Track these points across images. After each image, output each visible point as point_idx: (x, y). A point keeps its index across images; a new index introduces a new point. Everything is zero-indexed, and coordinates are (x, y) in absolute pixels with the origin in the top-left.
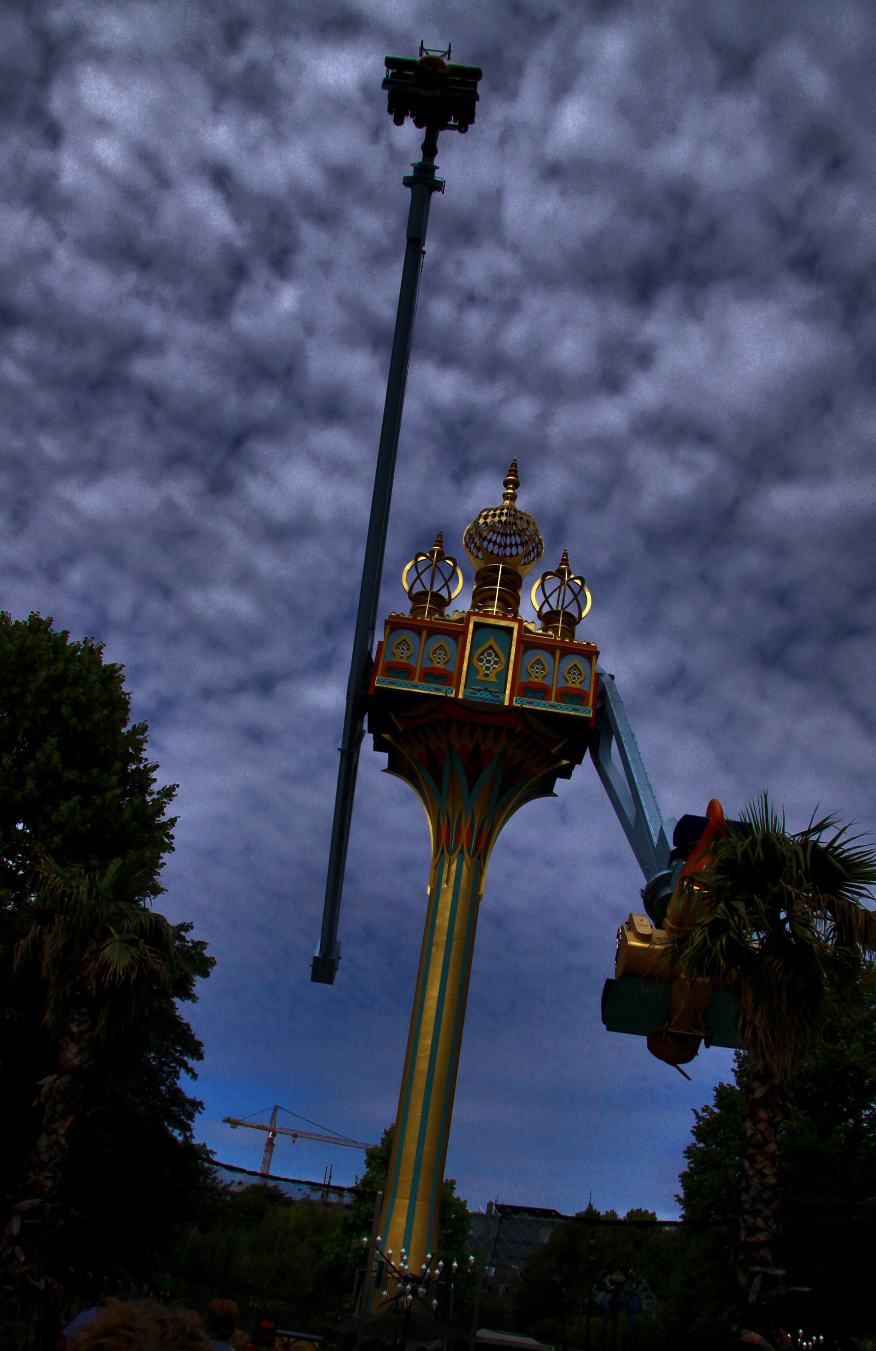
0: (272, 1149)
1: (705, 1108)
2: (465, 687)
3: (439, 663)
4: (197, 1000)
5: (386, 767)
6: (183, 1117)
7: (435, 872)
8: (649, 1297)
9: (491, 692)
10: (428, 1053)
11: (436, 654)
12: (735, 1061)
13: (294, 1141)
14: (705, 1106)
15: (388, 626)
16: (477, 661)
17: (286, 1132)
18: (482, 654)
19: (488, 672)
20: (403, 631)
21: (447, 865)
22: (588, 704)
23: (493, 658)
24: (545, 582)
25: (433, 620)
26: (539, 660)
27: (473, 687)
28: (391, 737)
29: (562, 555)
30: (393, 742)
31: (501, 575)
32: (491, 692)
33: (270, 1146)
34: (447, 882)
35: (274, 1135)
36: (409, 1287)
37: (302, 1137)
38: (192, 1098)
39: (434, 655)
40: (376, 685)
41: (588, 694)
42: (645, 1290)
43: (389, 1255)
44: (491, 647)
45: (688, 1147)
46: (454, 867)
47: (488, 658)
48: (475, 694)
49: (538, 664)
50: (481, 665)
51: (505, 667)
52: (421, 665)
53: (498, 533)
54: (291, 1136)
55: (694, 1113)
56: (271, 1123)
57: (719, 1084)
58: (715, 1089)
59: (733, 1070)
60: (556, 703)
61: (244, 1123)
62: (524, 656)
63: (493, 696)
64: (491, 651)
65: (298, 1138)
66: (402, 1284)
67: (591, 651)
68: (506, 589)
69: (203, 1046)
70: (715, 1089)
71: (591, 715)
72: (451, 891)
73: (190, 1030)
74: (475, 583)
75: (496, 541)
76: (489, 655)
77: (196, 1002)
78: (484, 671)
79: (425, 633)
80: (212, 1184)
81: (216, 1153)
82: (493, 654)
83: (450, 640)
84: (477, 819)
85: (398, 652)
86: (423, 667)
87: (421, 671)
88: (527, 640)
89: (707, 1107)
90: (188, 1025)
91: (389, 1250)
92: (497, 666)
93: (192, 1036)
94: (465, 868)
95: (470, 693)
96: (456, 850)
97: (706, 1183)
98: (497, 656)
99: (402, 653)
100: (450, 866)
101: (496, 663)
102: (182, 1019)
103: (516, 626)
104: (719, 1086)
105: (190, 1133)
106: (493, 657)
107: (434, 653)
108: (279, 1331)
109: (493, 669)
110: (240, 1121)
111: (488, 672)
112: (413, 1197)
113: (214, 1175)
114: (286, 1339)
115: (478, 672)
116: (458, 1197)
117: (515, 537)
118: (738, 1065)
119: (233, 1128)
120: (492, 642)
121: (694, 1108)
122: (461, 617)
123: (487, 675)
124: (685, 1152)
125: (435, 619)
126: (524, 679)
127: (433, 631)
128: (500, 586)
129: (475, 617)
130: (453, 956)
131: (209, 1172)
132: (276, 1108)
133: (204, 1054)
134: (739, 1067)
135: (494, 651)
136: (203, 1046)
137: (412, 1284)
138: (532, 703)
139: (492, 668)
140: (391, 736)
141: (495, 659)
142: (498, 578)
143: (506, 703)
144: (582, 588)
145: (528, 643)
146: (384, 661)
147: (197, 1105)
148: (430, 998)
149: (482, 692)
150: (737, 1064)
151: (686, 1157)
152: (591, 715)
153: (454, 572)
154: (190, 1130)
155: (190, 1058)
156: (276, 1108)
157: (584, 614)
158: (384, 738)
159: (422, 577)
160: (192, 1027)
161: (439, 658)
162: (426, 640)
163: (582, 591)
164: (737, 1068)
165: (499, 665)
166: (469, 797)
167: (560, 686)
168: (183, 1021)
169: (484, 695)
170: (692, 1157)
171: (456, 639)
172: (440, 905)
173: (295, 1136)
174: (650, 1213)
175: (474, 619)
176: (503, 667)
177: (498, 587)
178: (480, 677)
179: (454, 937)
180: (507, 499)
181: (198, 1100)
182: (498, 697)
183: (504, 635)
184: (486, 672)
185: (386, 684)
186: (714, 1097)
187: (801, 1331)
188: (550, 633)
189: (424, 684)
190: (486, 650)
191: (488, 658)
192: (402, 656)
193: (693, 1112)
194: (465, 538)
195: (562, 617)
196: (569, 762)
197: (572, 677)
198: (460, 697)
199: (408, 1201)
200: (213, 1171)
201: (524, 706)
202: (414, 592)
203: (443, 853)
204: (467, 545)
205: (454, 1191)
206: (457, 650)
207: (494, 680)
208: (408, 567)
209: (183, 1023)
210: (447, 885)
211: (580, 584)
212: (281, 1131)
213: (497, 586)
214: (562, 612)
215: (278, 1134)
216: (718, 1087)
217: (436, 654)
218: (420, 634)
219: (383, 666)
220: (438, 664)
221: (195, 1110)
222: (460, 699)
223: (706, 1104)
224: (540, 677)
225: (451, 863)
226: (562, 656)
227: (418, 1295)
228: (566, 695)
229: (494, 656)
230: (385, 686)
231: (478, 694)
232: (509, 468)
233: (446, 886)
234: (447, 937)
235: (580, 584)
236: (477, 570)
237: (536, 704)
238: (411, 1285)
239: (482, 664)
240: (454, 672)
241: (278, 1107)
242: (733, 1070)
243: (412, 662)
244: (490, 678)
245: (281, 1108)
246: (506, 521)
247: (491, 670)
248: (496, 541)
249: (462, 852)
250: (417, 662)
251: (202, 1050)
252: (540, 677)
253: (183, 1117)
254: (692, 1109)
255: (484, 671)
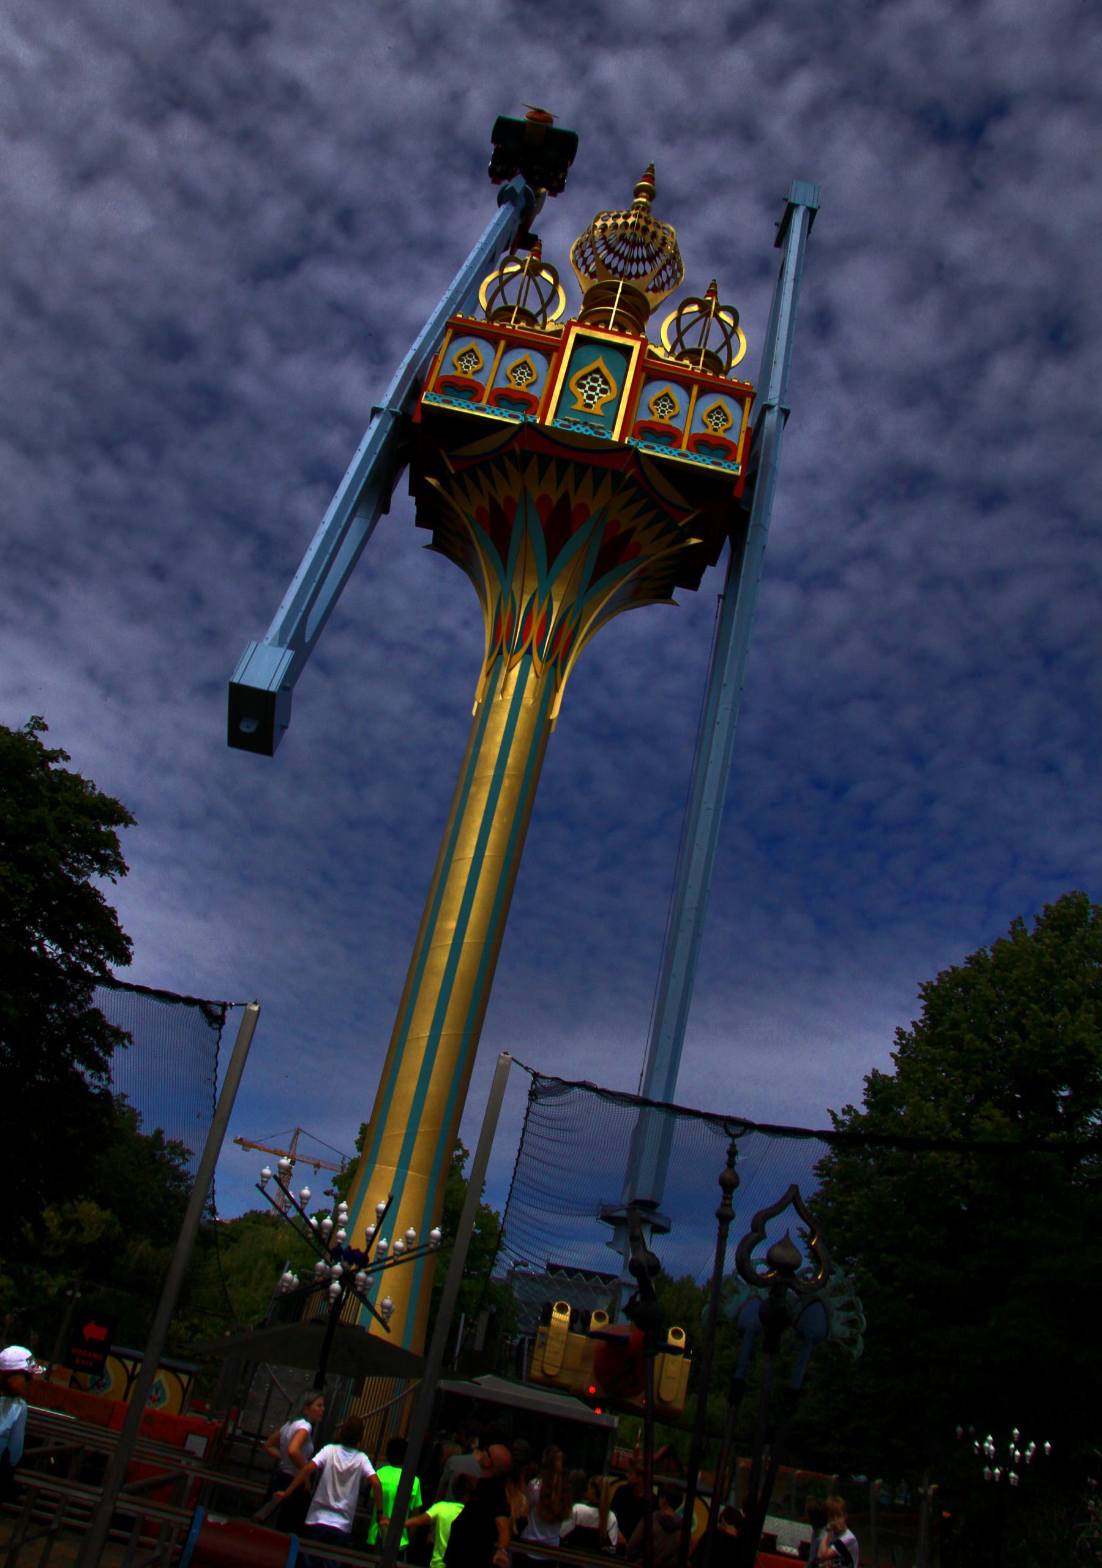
0: (289, 1179)
1: (847, 1109)
2: (555, 416)
3: (519, 384)
4: (126, 871)
5: (431, 542)
6: (96, 1049)
7: (486, 680)
8: (849, 1306)
9: (592, 427)
10: (450, 942)
11: (516, 372)
12: (895, 1042)
13: (316, 1172)
14: (847, 1106)
15: (450, 332)
16: (576, 387)
17: (307, 1161)
18: (585, 377)
19: (591, 402)
20: (467, 339)
21: (504, 670)
22: (735, 459)
23: (599, 385)
24: (682, 317)
25: (516, 328)
26: (667, 395)
27: (567, 417)
28: (438, 483)
29: (709, 285)
30: (441, 490)
31: (621, 294)
32: (592, 427)
33: (287, 1176)
34: (502, 692)
35: (292, 1163)
36: (338, 1267)
37: (326, 1168)
38: (115, 1026)
39: (513, 374)
40: (424, 401)
41: (736, 448)
42: (839, 1289)
43: (302, 1197)
44: (598, 371)
45: (820, 1162)
46: (515, 672)
47: (592, 384)
48: (569, 427)
49: (666, 401)
50: (581, 392)
51: (617, 396)
52: (493, 384)
53: (621, 257)
54: (313, 1166)
55: (831, 1115)
56: (291, 1147)
57: (871, 1071)
58: (867, 1079)
59: (892, 1055)
60: (688, 453)
61: (259, 1145)
62: (648, 387)
63: (596, 433)
64: (598, 376)
65: (321, 1168)
66: (327, 1262)
67: (744, 391)
68: (626, 313)
69: (132, 944)
70: (867, 1079)
71: (739, 473)
72: (507, 707)
73: (116, 919)
74: (582, 307)
75: (616, 267)
76: (595, 380)
77: (126, 875)
78: (585, 400)
79: (502, 343)
80: (187, 1192)
81: (194, 1154)
82: (600, 380)
83: (539, 357)
84: (556, 606)
85: (462, 365)
86: (495, 387)
87: (492, 392)
88: (648, 366)
89: (850, 1107)
90: (112, 912)
91: (304, 1188)
92: (604, 396)
93: (119, 929)
94: (532, 675)
95: (561, 425)
96: (521, 648)
97: (850, 1207)
98: (605, 382)
99: (467, 367)
100: (509, 670)
101: (603, 391)
102: (105, 900)
103: (637, 346)
104: (872, 1074)
105: (107, 1076)
106: (600, 382)
107: (514, 371)
108: (113, 1348)
109: (598, 399)
110: (254, 1142)
111: (591, 402)
112: (404, 1163)
113: (189, 1182)
114: (130, 1364)
115: (575, 399)
116: (487, 1205)
117: (644, 265)
118: (900, 1050)
119: (246, 1150)
120: (599, 363)
121: (830, 1109)
122: (558, 329)
123: (589, 406)
124: (815, 1168)
125: (519, 328)
126: (643, 416)
127: (515, 343)
128: (618, 307)
129: (578, 328)
130: (501, 802)
131: (184, 1178)
132: (298, 1132)
133: (133, 957)
134: (902, 1051)
135: (602, 376)
136: (132, 944)
137: (346, 1264)
138: (653, 448)
139: (596, 397)
140: (438, 481)
141: (603, 386)
142: (616, 297)
143: (615, 437)
144: (734, 329)
145: (650, 371)
146: (438, 374)
147: (120, 1036)
148: (458, 860)
149: (578, 426)
150: (899, 1047)
151: (817, 1175)
152: (739, 473)
153: (554, 294)
154: (107, 1070)
155: (115, 963)
156: (298, 1132)
157: (734, 362)
158: (429, 483)
159: (506, 289)
160: (118, 915)
161: (521, 379)
162: (504, 353)
163: (735, 334)
164: (899, 1053)
165: (608, 394)
166: (548, 574)
167: (694, 431)
168: (105, 904)
169: (582, 430)
170: (828, 1174)
171: (548, 356)
172: (489, 724)
173: (317, 1166)
174: (868, 1111)
175: (575, 330)
176: (615, 396)
177: (615, 309)
178: (579, 406)
179: (506, 772)
180: (638, 208)
181: (123, 1030)
182: (603, 434)
183: (619, 357)
184: (587, 401)
185: (438, 402)
186: (865, 1089)
187: (1016, 1431)
188: (686, 362)
189: (494, 408)
190: (590, 374)
191: (592, 384)
192: (467, 370)
193: (829, 1114)
194: (574, 253)
195: (704, 357)
196: (700, 541)
197: (713, 422)
198: (548, 422)
199: (395, 1169)
200: (189, 1177)
201: (640, 450)
202: (494, 309)
203: (500, 653)
204: (576, 263)
205: (483, 1194)
206: (548, 370)
207: (599, 412)
208: (488, 279)
209: (106, 907)
210: (502, 697)
211: (732, 325)
212: (301, 1159)
213: (613, 307)
214: (704, 351)
215: (297, 1162)
216: (871, 1076)
217: (516, 372)
218: (495, 345)
219: (437, 380)
220: (520, 384)
221: (117, 1043)
222: (547, 426)
223: (848, 1104)
224: (667, 418)
225: (511, 666)
226: (701, 393)
227: (356, 1286)
228: (700, 444)
229: (602, 382)
230: (436, 405)
231: (574, 428)
232: (644, 174)
233: (501, 698)
234: (495, 772)
235: (732, 325)
236: (585, 292)
237: (657, 449)
238: (342, 1265)
239: (583, 391)
240: (540, 398)
241: (301, 1130)
242: (892, 1055)
243: (478, 379)
244: (593, 409)
245: (304, 1132)
246: (633, 223)
247: (596, 400)
248: (616, 267)
249: (529, 652)
250: (487, 381)
251: (130, 951)
252: (667, 418)
253: (96, 1049)
254: (829, 1110)
255: (585, 400)
